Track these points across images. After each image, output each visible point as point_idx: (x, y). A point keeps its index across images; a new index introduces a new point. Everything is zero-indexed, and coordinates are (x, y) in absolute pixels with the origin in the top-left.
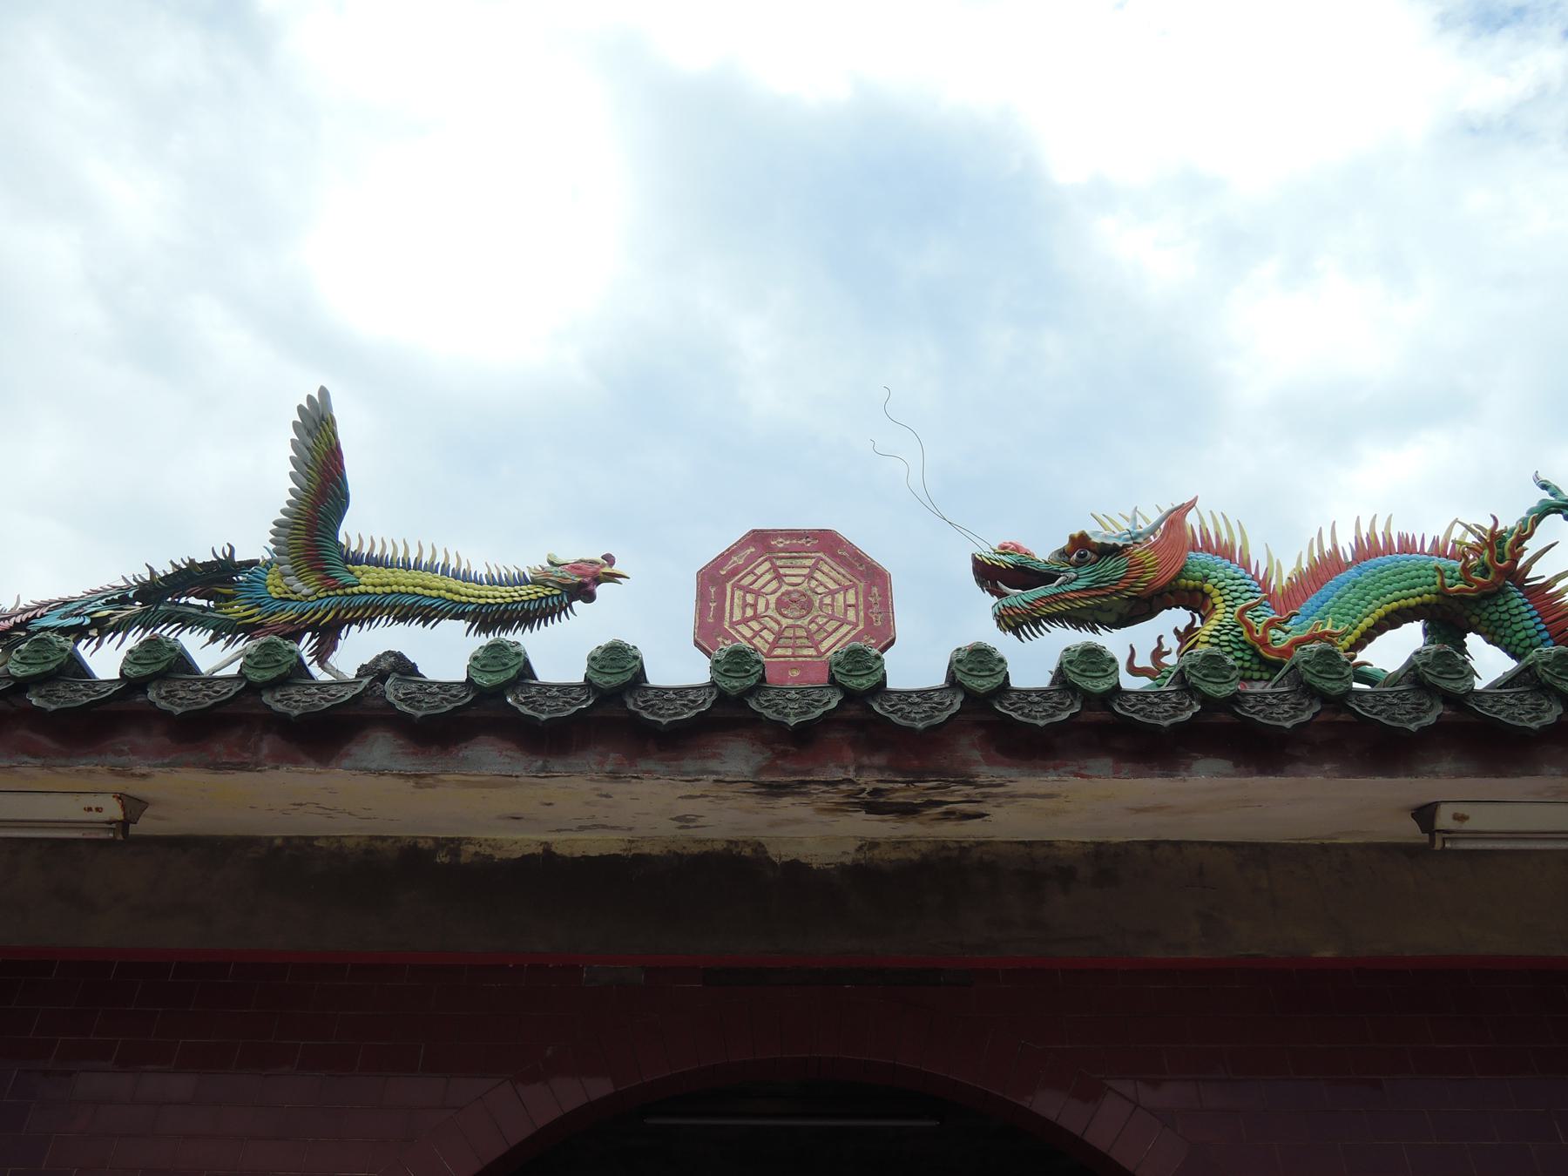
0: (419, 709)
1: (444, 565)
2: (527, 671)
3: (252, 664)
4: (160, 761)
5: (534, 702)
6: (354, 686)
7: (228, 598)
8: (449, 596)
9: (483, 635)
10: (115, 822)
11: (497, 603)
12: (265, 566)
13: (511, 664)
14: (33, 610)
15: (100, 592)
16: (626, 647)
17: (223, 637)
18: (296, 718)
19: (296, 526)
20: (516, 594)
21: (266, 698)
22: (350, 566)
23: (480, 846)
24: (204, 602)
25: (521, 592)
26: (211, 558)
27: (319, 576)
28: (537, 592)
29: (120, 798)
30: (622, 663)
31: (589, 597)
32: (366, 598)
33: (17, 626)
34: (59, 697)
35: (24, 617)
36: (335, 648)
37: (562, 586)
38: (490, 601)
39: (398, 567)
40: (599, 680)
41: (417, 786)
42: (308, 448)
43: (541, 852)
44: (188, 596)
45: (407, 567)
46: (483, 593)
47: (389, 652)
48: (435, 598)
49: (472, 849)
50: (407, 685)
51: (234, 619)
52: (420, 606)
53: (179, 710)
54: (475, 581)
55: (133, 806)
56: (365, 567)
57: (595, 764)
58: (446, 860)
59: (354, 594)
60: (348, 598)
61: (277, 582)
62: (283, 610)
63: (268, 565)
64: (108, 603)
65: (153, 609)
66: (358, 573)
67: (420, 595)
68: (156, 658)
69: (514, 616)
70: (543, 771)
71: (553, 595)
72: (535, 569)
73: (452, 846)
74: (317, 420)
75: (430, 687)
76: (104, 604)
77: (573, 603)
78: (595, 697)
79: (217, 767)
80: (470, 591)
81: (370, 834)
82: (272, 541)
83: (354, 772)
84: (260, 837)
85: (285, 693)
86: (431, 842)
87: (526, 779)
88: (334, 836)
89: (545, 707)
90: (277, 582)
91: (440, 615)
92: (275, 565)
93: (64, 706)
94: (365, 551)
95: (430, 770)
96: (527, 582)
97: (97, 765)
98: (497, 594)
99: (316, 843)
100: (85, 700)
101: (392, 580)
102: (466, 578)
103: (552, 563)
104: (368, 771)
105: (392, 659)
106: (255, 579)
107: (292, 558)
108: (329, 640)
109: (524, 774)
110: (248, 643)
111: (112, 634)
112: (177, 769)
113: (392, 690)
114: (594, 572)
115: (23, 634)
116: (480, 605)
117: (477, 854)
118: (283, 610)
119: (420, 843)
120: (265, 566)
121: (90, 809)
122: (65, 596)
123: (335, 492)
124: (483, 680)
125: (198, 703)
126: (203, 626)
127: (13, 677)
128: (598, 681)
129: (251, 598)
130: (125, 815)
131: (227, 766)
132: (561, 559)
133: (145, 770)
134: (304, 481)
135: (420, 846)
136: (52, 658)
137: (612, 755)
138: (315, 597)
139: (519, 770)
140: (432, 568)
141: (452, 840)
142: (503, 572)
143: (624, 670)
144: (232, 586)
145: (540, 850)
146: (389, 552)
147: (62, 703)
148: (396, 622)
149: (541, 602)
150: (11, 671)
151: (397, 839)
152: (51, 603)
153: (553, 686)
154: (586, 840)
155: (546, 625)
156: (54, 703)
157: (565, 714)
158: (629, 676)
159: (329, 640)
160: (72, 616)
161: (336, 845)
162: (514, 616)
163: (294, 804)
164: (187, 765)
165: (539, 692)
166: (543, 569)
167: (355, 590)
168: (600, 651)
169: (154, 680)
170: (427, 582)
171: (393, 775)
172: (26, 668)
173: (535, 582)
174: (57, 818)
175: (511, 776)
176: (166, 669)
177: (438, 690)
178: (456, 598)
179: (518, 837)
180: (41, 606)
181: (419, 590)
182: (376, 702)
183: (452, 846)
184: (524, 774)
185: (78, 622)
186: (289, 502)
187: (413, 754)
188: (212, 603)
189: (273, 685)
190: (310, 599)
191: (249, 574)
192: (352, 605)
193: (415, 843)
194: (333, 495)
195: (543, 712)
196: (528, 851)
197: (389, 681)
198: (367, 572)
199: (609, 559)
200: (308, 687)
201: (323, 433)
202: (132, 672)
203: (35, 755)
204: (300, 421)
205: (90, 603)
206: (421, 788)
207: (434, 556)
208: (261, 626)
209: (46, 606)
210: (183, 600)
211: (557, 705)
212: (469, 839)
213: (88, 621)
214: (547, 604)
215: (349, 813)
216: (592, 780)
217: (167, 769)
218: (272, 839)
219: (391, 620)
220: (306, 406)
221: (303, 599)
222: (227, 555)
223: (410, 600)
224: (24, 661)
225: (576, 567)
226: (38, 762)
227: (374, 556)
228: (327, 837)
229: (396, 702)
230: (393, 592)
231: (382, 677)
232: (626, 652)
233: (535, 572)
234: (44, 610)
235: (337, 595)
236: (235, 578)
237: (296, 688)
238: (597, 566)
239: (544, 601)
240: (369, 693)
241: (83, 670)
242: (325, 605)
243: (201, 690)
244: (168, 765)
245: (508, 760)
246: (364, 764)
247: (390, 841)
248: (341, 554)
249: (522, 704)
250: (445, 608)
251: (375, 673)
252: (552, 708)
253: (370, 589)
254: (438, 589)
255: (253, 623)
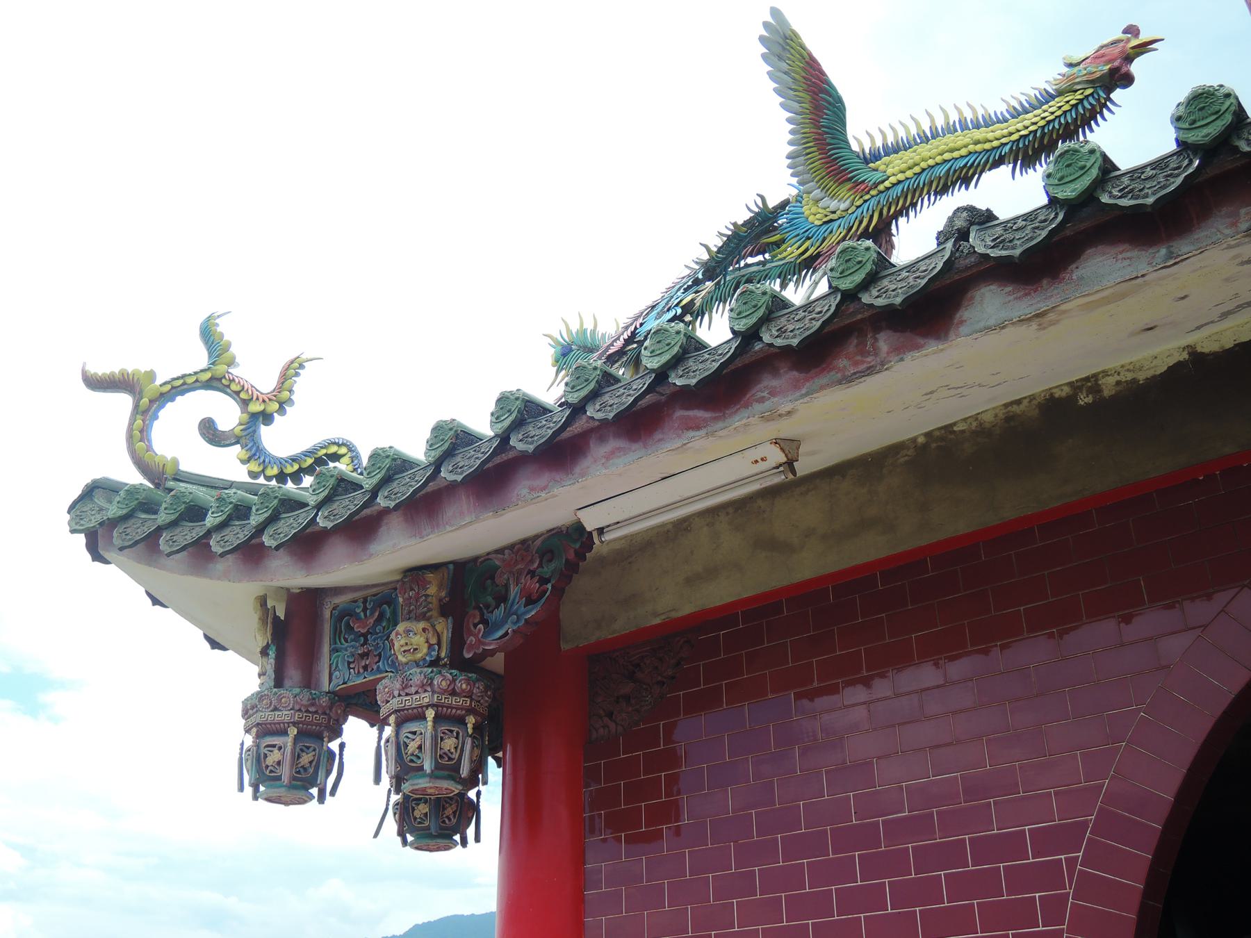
0: (1014, 248)
1: (960, 121)
2: (1108, 166)
3: (838, 275)
4: (798, 394)
5: (1132, 191)
6: (939, 255)
7: (778, 244)
8: (979, 147)
9: (1031, 171)
10: (781, 465)
11: (1031, 132)
12: (797, 201)
13: (1089, 165)
14: (632, 324)
15: (673, 287)
16: (1211, 89)
17: (790, 280)
18: (900, 305)
19: (808, 151)
20: (1046, 114)
21: (866, 298)
22: (871, 165)
23: (1119, 374)
24: (760, 258)
25: (1051, 110)
26: (748, 215)
27: (849, 185)
28: (1068, 102)
29: (776, 443)
30: (1217, 108)
31: (1126, 80)
32: (900, 187)
33: (629, 341)
34: (694, 372)
35: (629, 332)
36: (893, 247)
37: (1092, 82)
38: (1023, 133)
39: (917, 144)
40: (1194, 137)
41: (1042, 327)
42: (785, 73)
43: (1187, 357)
44: (744, 258)
45: (925, 139)
46: (1012, 129)
47: (958, 209)
48: (967, 156)
49: (1111, 380)
50: (990, 231)
51: (792, 260)
52: (955, 171)
53: (795, 342)
54: (999, 122)
55: (789, 446)
56: (885, 159)
57: (1226, 227)
58: (1090, 399)
59: (888, 189)
60: (884, 194)
61: (814, 210)
62: (831, 232)
63: (799, 198)
64: (686, 290)
65: (722, 282)
66: (882, 167)
67: (951, 160)
68: (754, 306)
69: (1054, 136)
70: (1171, 258)
71: (1087, 97)
72: (1055, 80)
73: (1089, 384)
74: (781, 41)
75: (1015, 223)
76: (683, 293)
77: (1112, 96)
78: (1199, 156)
79: (848, 380)
80: (998, 134)
81: (1003, 402)
82: (793, 175)
83: (975, 336)
84: (903, 442)
85: (879, 288)
86: (1067, 390)
87: (1155, 274)
88: (970, 417)
89: (1146, 191)
90: (814, 210)
91: (978, 171)
92: (804, 196)
93: (701, 377)
94: (879, 143)
95: (1050, 304)
96: (1053, 97)
97: (749, 417)
98: (1027, 123)
99: (955, 428)
100: (716, 365)
101: (917, 158)
102: (988, 123)
103: (1071, 65)
104: (989, 329)
105: (965, 214)
106: (796, 216)
107: (817, 182)
108: (884, 241)
109: (1151, 269)
110: (814, 277)
111: (700, 317)
112: (814, 395)
113: (979, 242)
114: (1122, 52)
115: (635, 346)
116: (1014, 142)
117: (1118, 383)
118: (831, 232)
119: (1055, 393)
120: (797, 201)
121: (756, 462)
122: (650, 303)
123: (829, 103)
124: (1068, 192)
125: (808, 329)
126: (769, 279)
127: (653, 370)
128: (1194, 138)
129: (798, 235)
130: (786, 456)
131: (857, 375)
132: (1078, 56)
133: (788, 407)
134: (796, 105)
135: (1057, 396)
136: (673, 343)
137: (1243, 211)
138: (853, 208)
139: (1143, 268)
140: (949, 129)
141: (1087, 379)
142: (1023, 99)
143: (1219, 115)
144: (777, 232)
145: (1185, 356)
146: (902, 134)
147: (699, 375)
148: (939, 197)
149: (1077, 109)
150: (648, 366)
151: (1032, 398)
152: (642, 313)
153: (1145, 167)
154: (1232, 328)
155: (1104, 119)
156: (694, 377)
157: (1172, 188)
158: (1228, 118)
159: (884, 241)
160: (665, 313)
161: (974, 424)
162: (1054, 136)
163: (926, 394)
164: (822, 388)
165: (1132, 180)
166: (1064, 75)
167: (887, 184)
168: (1182, 108)
169: (761, 326)
170: (951, 145)
171: (1013, 324)
172: (657, 359)
173: (1060, 93)
174: (733, 479)
175: (1137, 277)
176: (767, 312)
177: (1024, 223)
178: (987, 146)
179: (1156, 350)
180: (636, 319)
181: (947, 156)
182: (967, 261)
183: (1089, 384)
184: (1151, 269)
185: (672, 316)
186: (792, 132)
187: (1026, 295)
188: (767, 256)
189: (866, 285)
190: (850, 212)
191: (787, 214)
192: (891, 200)
193: (1052, 395)
194: (828, 105)
195: (1146, 196)
196: (1172, 362)
197: (972, 235)
198: (890, 162)
199: (1132, 30)
200: (898, 273)
201: (792, 51)
202: (742, 326)
203: (698, 428)
204: (768, 51)
205: (672, 297)
206: (1044, 328)
207: (947, 117)
208: (819, 255)
209: (639, 316)
210: (742, 263)
211: (1159, 183)
212: (1103, 372)
213: (679, 311)
214: (1084, 108)
215: (980, 385)
216: (1230, 247)
217: (806, 399)
218: (914, 440)
219: (932, 198)
220: (765, 34)
221: (844, 214)
222: (762, 207)
223: (941, 171)
224: (653, 354)
225: (1098, 56)
226: (702, 432)
227: (890, 145)
228: (965, 420)
229: (989, 251)
230: (923, 170)
231: (963, 235)
232: (1213, 95)
233: (1057, 82)
234: (641, 320)
235: (873, 196)
236: (775, 224)
237: (888, 279)
238: (1122, 44)
239: (1080, 108)
240: (957, 255)
241: (700, 344)
242: (868, 211)
243: (805, 317)
244: (807, 394)
245: (1127, 262)
246: (982, 325)
247: (1025, 402)
248: (858, 156)
249: (1121, 197)
250: (981, 161)
251: (954, 234)
252: (1155, 189)
253: (901, 177)
254: (966, 146)
255: (811, 256)
